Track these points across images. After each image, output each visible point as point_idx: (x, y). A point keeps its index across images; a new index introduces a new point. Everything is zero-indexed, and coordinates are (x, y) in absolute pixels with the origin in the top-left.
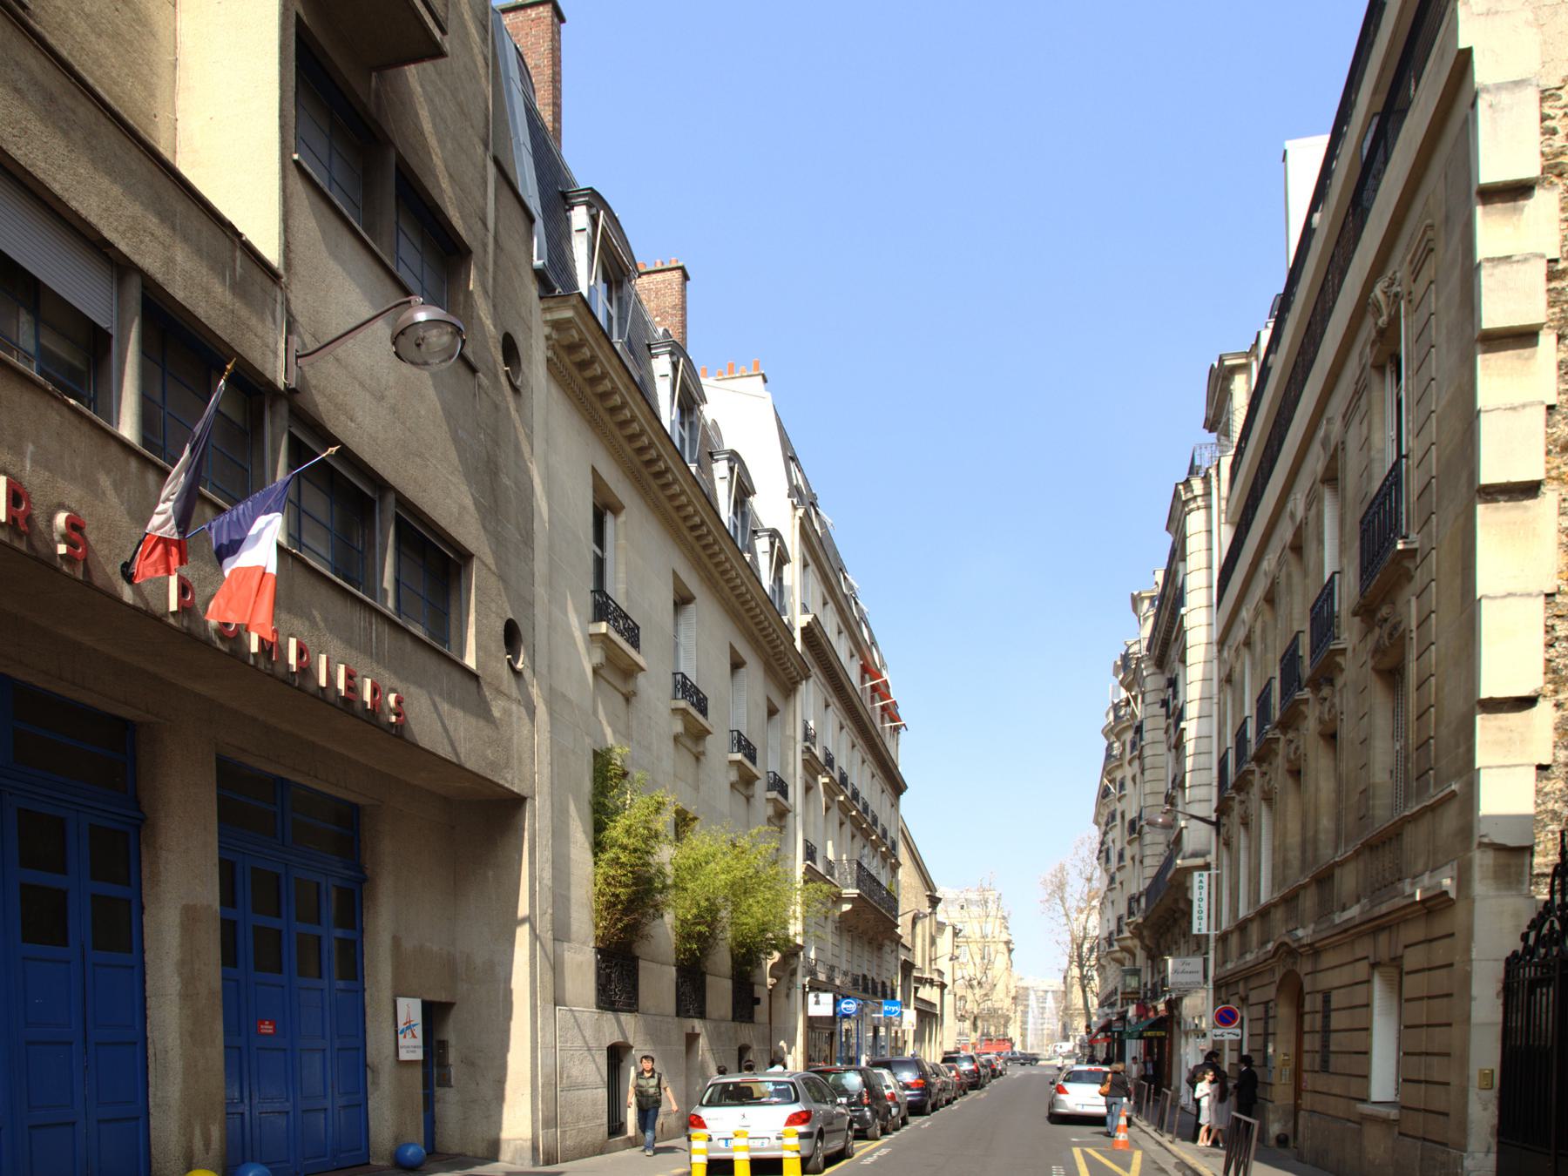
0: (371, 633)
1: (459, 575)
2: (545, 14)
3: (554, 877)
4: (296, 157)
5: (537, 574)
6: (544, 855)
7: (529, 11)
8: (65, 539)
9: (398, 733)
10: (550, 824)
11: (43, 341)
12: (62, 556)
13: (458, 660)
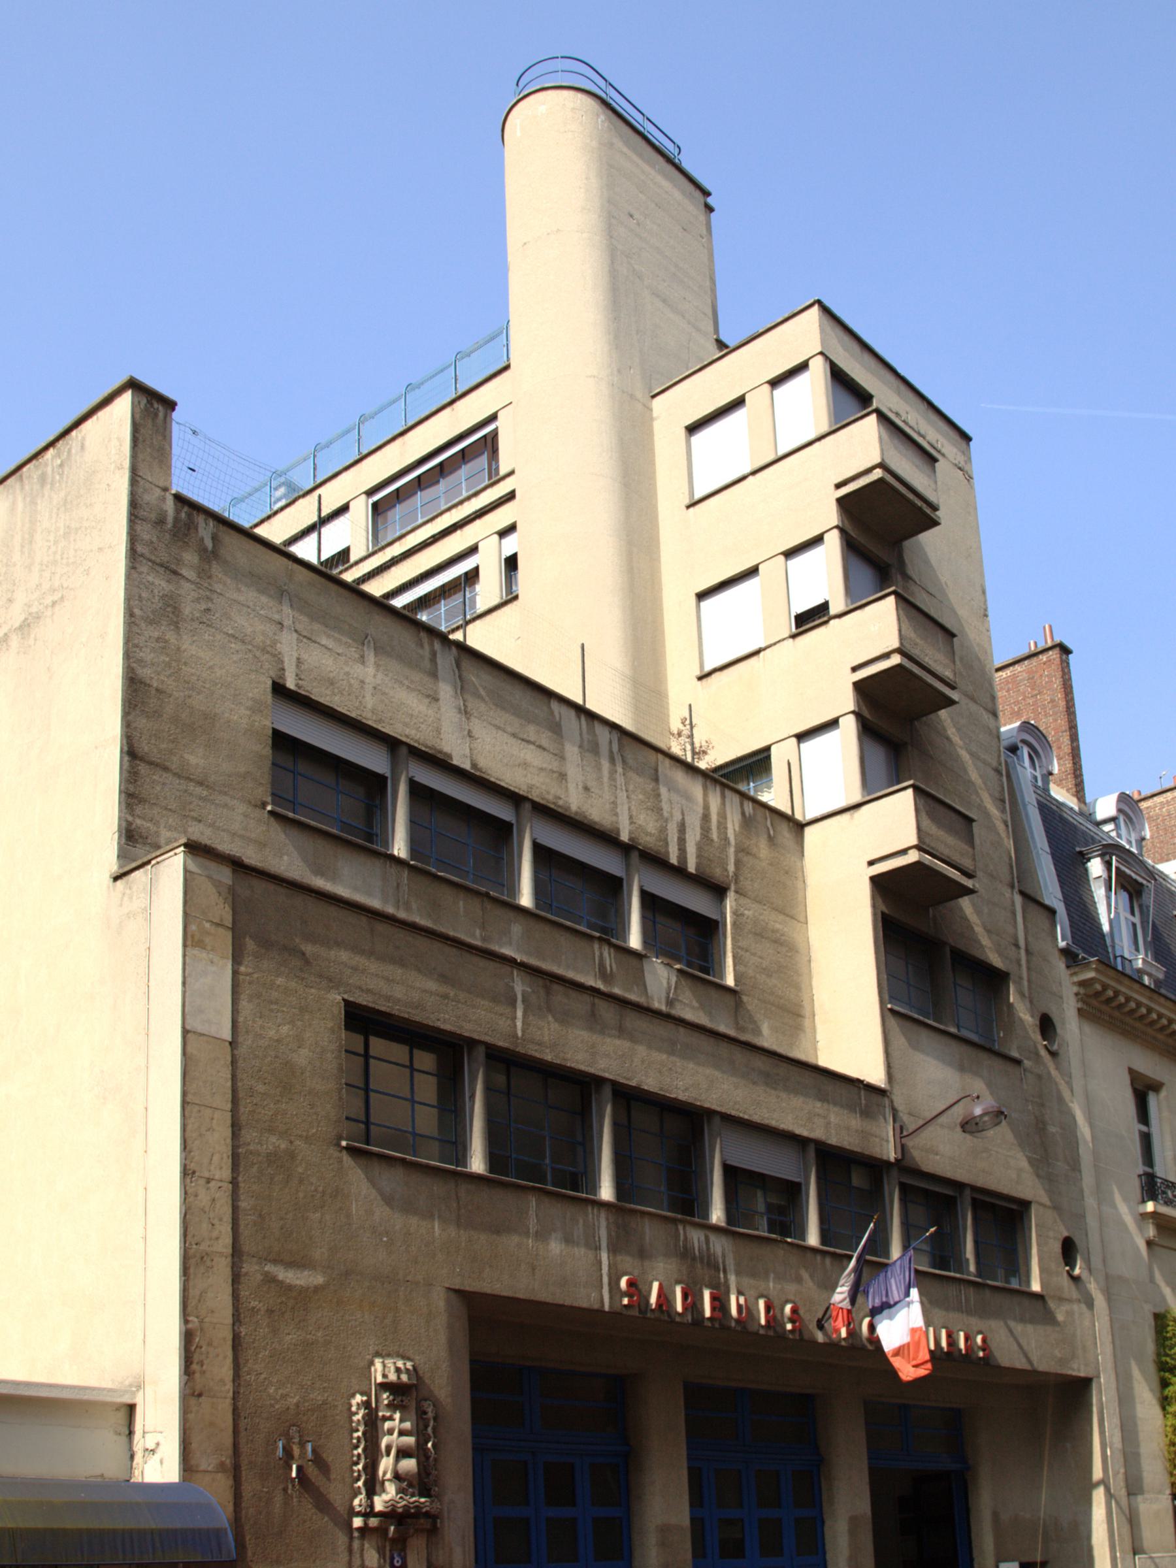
1: (1022, 1219)
2: (1054, 656)
3: (1123, 1439)
4: (889, 1006)
5: (1085, 1189)
6: (1112, 1423)
7: (1040, 657)
8: (792, 1320)
9: (988, 1362)
10: (1116, 1395)
11: (768, 1200)
12: (789, 1331)
13: (1024, 1288)
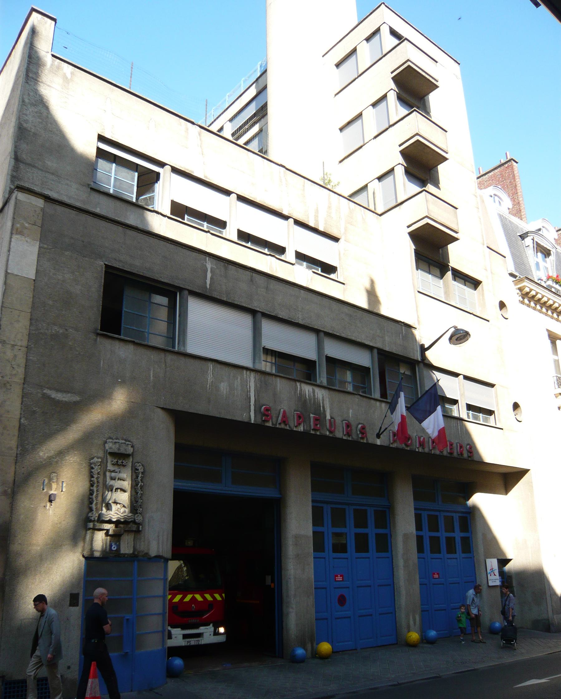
0: (458, 427)
